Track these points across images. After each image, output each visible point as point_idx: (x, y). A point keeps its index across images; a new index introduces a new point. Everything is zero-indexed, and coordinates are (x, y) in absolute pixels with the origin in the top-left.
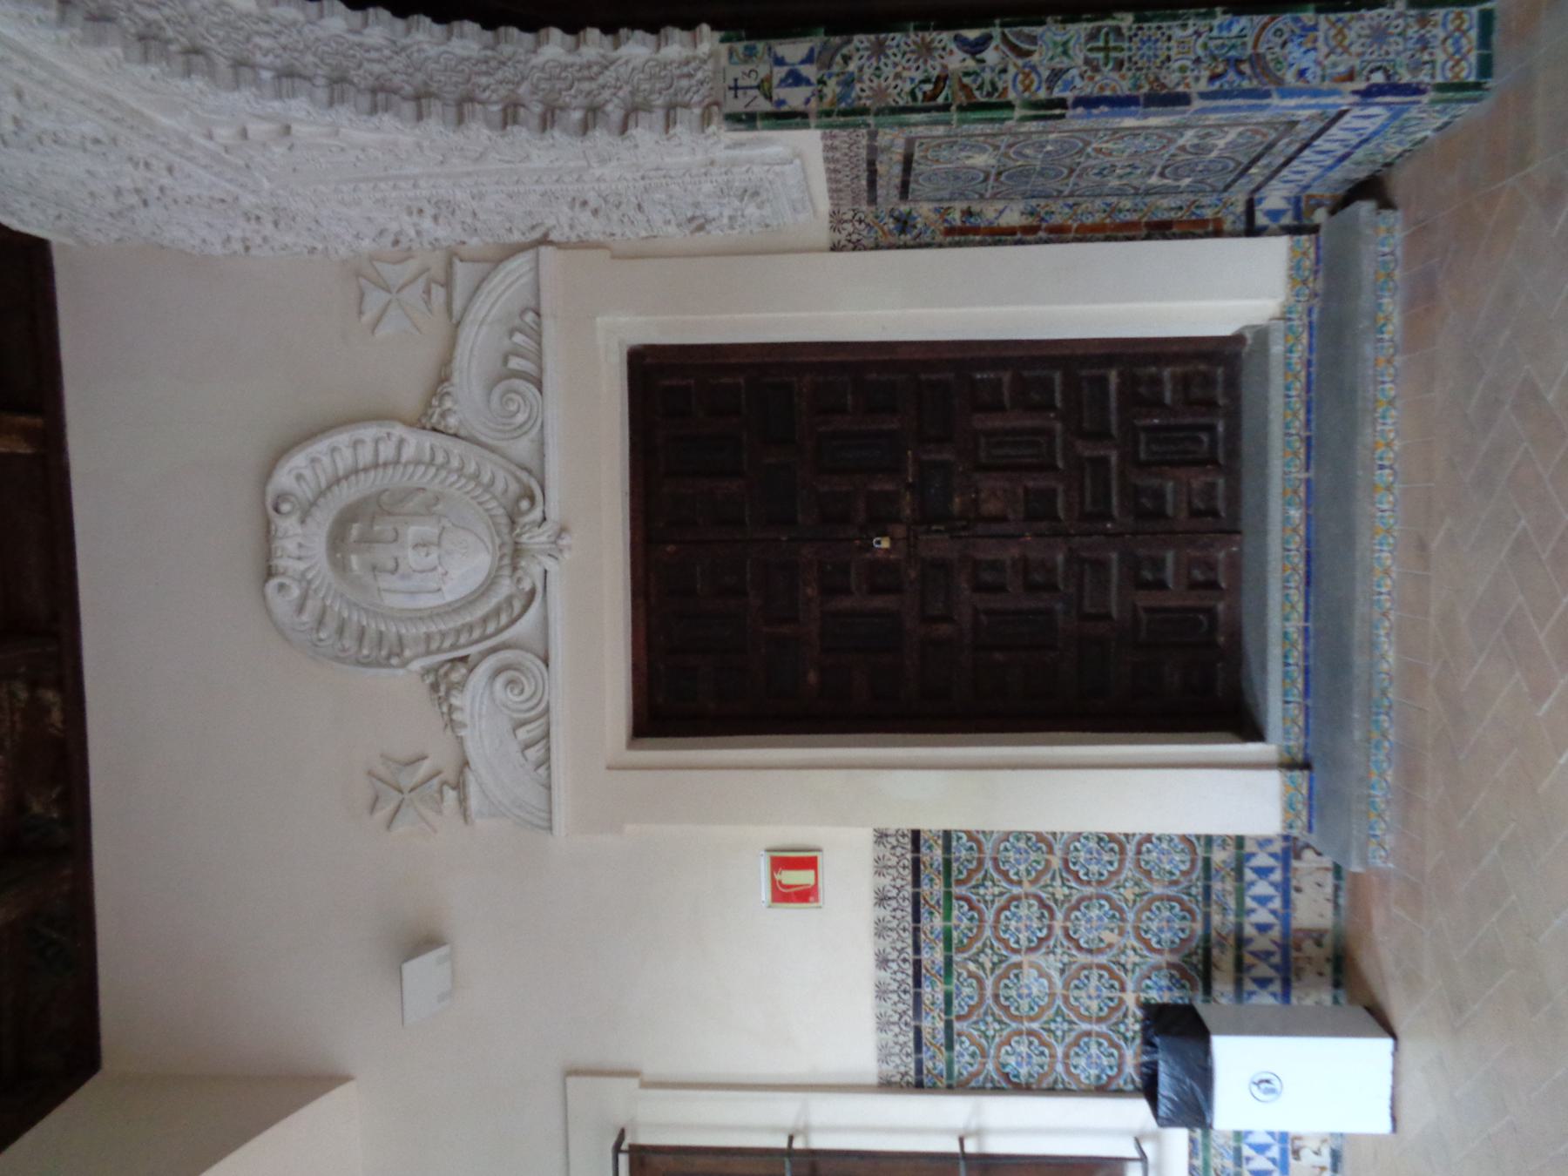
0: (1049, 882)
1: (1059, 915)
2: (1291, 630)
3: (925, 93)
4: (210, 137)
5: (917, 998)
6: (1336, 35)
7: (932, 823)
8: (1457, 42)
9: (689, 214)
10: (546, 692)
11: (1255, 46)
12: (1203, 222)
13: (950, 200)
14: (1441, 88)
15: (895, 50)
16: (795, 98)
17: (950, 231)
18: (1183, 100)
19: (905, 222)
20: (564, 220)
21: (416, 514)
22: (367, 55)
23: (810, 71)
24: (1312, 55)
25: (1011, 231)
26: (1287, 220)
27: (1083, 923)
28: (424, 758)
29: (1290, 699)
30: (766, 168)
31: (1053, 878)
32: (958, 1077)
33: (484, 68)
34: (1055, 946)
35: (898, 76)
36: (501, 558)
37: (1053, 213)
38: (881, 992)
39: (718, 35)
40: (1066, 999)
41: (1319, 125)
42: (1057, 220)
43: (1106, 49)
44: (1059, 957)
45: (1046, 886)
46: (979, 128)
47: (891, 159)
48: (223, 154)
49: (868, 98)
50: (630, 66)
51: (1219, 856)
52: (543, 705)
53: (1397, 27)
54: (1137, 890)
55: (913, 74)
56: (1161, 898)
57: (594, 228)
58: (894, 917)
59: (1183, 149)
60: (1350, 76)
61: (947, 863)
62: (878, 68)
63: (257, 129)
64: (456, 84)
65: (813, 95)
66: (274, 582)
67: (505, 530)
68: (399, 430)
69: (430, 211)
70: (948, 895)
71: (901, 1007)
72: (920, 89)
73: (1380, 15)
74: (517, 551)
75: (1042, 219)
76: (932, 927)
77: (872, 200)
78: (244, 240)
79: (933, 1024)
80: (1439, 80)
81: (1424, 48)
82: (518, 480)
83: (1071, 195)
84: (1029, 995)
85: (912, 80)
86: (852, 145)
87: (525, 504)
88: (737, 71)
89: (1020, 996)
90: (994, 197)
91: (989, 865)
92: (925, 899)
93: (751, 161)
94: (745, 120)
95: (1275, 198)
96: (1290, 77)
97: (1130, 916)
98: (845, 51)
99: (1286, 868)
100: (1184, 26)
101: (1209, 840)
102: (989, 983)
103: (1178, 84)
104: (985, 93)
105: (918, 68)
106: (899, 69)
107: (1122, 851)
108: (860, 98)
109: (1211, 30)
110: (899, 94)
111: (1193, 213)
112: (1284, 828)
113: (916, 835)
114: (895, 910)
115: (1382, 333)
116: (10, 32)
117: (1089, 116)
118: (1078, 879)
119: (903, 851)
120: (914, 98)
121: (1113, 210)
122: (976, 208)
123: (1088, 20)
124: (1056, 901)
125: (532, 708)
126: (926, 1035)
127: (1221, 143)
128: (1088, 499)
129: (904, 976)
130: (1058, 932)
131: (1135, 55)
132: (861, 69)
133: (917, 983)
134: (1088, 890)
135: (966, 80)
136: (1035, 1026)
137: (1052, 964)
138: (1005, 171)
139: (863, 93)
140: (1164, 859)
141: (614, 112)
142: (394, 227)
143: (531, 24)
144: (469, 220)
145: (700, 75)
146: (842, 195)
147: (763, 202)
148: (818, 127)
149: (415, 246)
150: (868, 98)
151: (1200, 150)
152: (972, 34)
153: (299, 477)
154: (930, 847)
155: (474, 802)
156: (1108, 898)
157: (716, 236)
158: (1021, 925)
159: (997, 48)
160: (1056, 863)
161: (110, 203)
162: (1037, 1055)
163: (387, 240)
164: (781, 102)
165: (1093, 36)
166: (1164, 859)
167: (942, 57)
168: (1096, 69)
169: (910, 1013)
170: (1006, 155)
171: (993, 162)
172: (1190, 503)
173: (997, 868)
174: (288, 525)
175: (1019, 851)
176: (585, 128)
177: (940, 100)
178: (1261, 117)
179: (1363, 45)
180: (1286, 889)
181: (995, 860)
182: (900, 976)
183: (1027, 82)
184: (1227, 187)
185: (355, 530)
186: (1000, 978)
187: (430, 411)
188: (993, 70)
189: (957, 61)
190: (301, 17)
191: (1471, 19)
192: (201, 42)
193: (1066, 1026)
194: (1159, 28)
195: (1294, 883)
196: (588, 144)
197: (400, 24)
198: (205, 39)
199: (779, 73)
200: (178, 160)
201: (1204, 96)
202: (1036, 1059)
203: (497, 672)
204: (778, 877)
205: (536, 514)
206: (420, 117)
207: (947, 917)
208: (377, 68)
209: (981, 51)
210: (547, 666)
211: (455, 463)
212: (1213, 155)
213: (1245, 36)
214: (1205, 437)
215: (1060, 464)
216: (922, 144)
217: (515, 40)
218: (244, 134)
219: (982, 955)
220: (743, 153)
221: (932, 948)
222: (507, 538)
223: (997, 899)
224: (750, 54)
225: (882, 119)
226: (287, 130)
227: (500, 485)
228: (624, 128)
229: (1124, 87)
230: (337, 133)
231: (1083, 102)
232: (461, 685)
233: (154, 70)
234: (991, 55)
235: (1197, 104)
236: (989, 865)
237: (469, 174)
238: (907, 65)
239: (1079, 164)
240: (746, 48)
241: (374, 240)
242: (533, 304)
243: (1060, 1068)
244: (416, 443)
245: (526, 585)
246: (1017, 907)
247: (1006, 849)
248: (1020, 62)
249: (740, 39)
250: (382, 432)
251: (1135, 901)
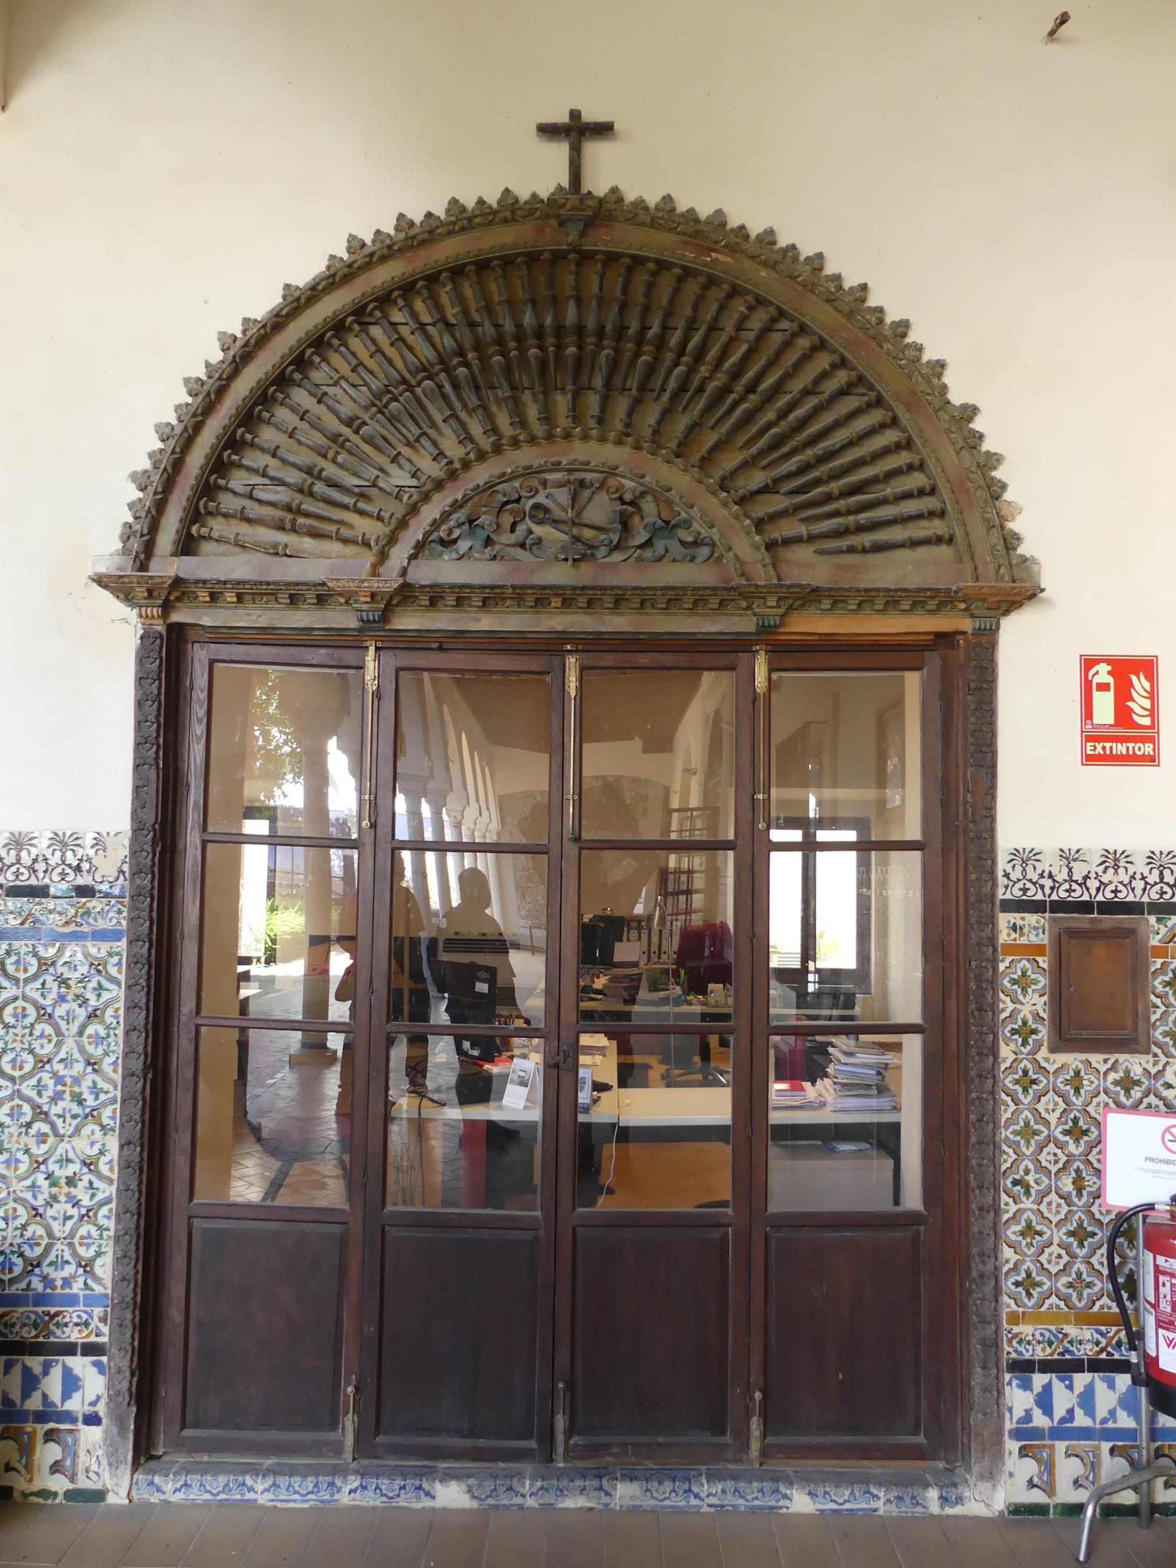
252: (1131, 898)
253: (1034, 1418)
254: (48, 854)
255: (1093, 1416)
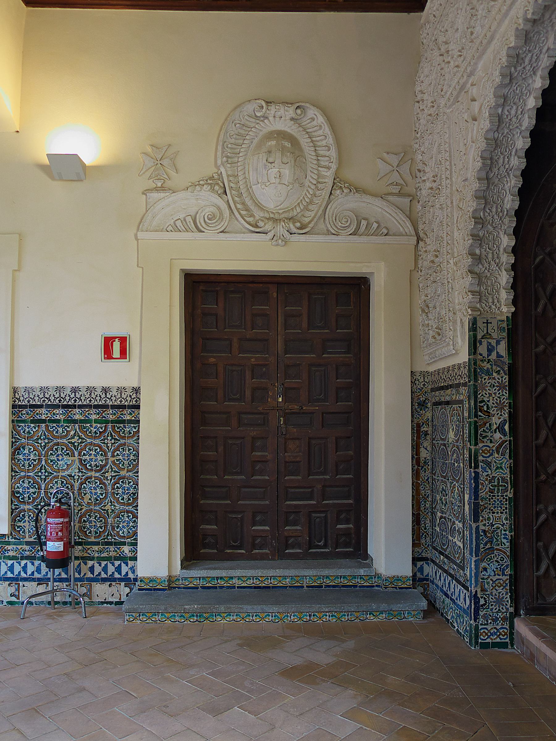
0: (114, 470)
1: (97, 475)
2: (234, 581)
3: (483, 406)
4: (472, 85)
5: (57, 407)
6: (500, 584)
7: (144, 414)
8: (495, 634)
9: (430, 305)
10: (209, 231)
11: (497, 549)
12: (419, 538)
13: (433, 425)
14: (477, 627)
15: (501, 394)
16: (482, 349)
17: (419, 426)
18: (476, 520)
19: (423, 406)
20: (429, 248)
21: (294, 174)
22: (506, 157)
23: (494, 356)
24: (493, 574)
25: (418, 453)
26: (419, 575)
27: (94, 486)
28: (177, 173)
29: (201, 580)
30: (451, 338)
31: (115, 472)
32: (18, 425)
33: (499, 210)
34: (82, 472)
35: (490, 395)
36: (272, 213)
37: (425, 472)
38: (59, 389)
39: (510, 315)
40: (57, 477)
41: (462, 580)
42: (422, 474)
43: (498, 485)
44: (77, 474)
45: (112, 469)
46: (466, 431)
47: (453, 395)
48: (464, 91)
49: (481, 381)
50: (498, 276)
51: (126, 549)
52: (203, 230)
53: (502, 608)
54: (110, 511)
55: (491, 401)
56: (106, 523)
57: (424, 263)
58: (97, 396)
59: (454, 523)
60: (483, 590)
61: (123, 422)
62: (494, 386)
63: (476, 106)
64: (492, 197)
65: (484, 357)
66: (264, 104)
67: (286, 215)
68: (334, 166)
69: (434, 185)
70: (107, 422)
71: (52, 398)
72: (484, 405)
73: (508, 601)
74: (276, 221)
75: (422, 467)
76: (91, 414)
77: (433, 390)
78: (423, 100)
79: (44, 414)
80: (480, 627)
81: (493, 620)
82: (310, 222)
83: (433, 479)
84: (58, 460)
85: (488, 401)
86: (461, 376)
87: (298, 225)
88: (495, 324)
89: (58, 455)
90: (433, 445)
91: (122, 441)
92: (105, 411)
93: (455, 330)
94: (473, 327)
95: (429, 570)
96: (483, 564)
97: (97, 508)
98: (502, 372)
99: (121, 580)
100: (506, 519)
101: (135, 544)
102: (65, 441)
103: (483, 517)
104: (481, 433)
105: (493, 404)
106: (493, 396)
107: (129, 504)
108: (481, 378)
109: (504, 530)
110: (482, 395)
111: (423, 534)
112: (140, 578)
113: (138, 407)
114: (100, 396)
115: (370, 615)
116: (517, 4)
117: (471, 479)
118: (116, 483)
119: (129, 401)
120: (481, 402)
121: (425, 498)
122: (428, 437)
123: (510, 478)
124: (104, 473)
125: (200, 223)
126: (38, 410)
127: (455, 540)
128: (293, 490)
129: (67, 400)
130: (89, 474)
131: (496, 498)
132: (494, 378)
133: (64, 407)
134: (110, 488)
135: (488, 425)
136: (43, 463)
137: (74, 471)
138: (446, 447)
139: (484, 380)
140: (125, 524)
141: (479, 269)
142: (427, 169)
143: (516, 232)
144: (430, 204)
145: (493, 307)
146: (436, 376)
147: (435, 338)
148: (469, 359)
149: (418, 180)
150: (481, 381)
151: (453, 531)
152: (507, 427)
153: (313, 119)
154: (130, 414)
155: (155, 195)
156: (106, 497)
157: (420, 318)
158: (92, 457)
159: (501, 438)
160: (123, 473)
161: (441, 39)
162: (29, 463)
163: (421, 167)
164: (481, 344)
165: (503, 479)
166: (125, 524)
167: (497, 414)
168: (490, 482)
169: (49, 403)
170: (454, 446)
171: (450, 441)
172: (292, 537)
173: (121, 445)
174: (291, 112)
175: (129, 456)
176: (472, 254)
177: (480, 413)
178: (467, 555)
179: (496, 595)
180: (111, 580)
181: (125, 444)
182: (68, 398)
183: (486, 452)
184: (434, 548)
185: (288, 144)
186: (67, 446)
187: (342, 183)
188: (491, 436)
189: (495, 421)
190: (523, 128)
191: (504, 639)
192: (514, 82)
193: (43, 477)
194: (506, 508)
195: (114, 583)
196: (465, 256)
197: (519, 173)
198: (516, 84)
199: (493, 342)
200: (462, 70)
201: (477, 528)
202: (27, 463)
203: (219, 208)
204: (117, 340)
205: (294, 230)
206: (479, 179)
207: (96, 421)
208: (501, 161)
209: (499, 431)
210: (221, 232)
211: (318, 193)
212: (450, 538)
213: (502, 545)
214: (321, 543)
215: (311, 477)
216: (460, 407)
217: (510, 223)
218: (473, 100)
219: (78, 438)
220: (459, 328)
221: (81, 414)
222: (283, 216)
223: (105, 445)
224: (501, 329)
225: (472, 387)
226: (475, 119)
227: (308, 214)
228: (471, 272)
229: (482, 494)
230: (473, 142)
231: (477, 474)
232: (213, 190)
233: (504, 59)
234: (498, 435)
235: (474, 526)
236: (122, 441)
237: (452, 203)
238: (495, 399)
239: (448, 480)
240: (504, 328)
241: (421, 161)
242: (390, 233)
243: (23, 474)
244: (329, 175)
245: (261, 224)
246: (102, 455)
247: (129, 450)
248: (494, 449)
249: (508, 325)
250: (334, 159)
251: (105, 510)
252: (34, 403)
253: (8, 574)
254: (86, 393)
255: (13, 573)
